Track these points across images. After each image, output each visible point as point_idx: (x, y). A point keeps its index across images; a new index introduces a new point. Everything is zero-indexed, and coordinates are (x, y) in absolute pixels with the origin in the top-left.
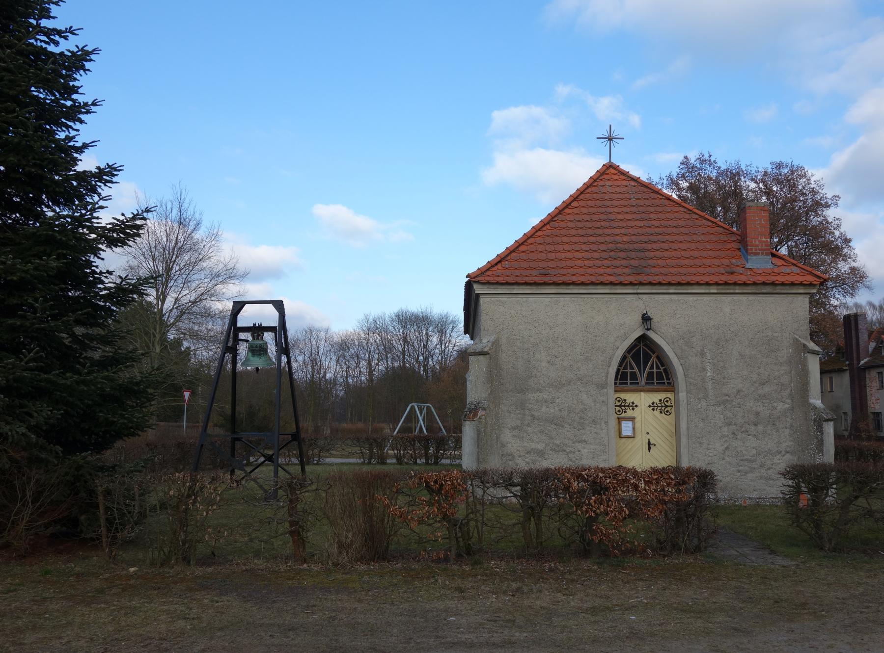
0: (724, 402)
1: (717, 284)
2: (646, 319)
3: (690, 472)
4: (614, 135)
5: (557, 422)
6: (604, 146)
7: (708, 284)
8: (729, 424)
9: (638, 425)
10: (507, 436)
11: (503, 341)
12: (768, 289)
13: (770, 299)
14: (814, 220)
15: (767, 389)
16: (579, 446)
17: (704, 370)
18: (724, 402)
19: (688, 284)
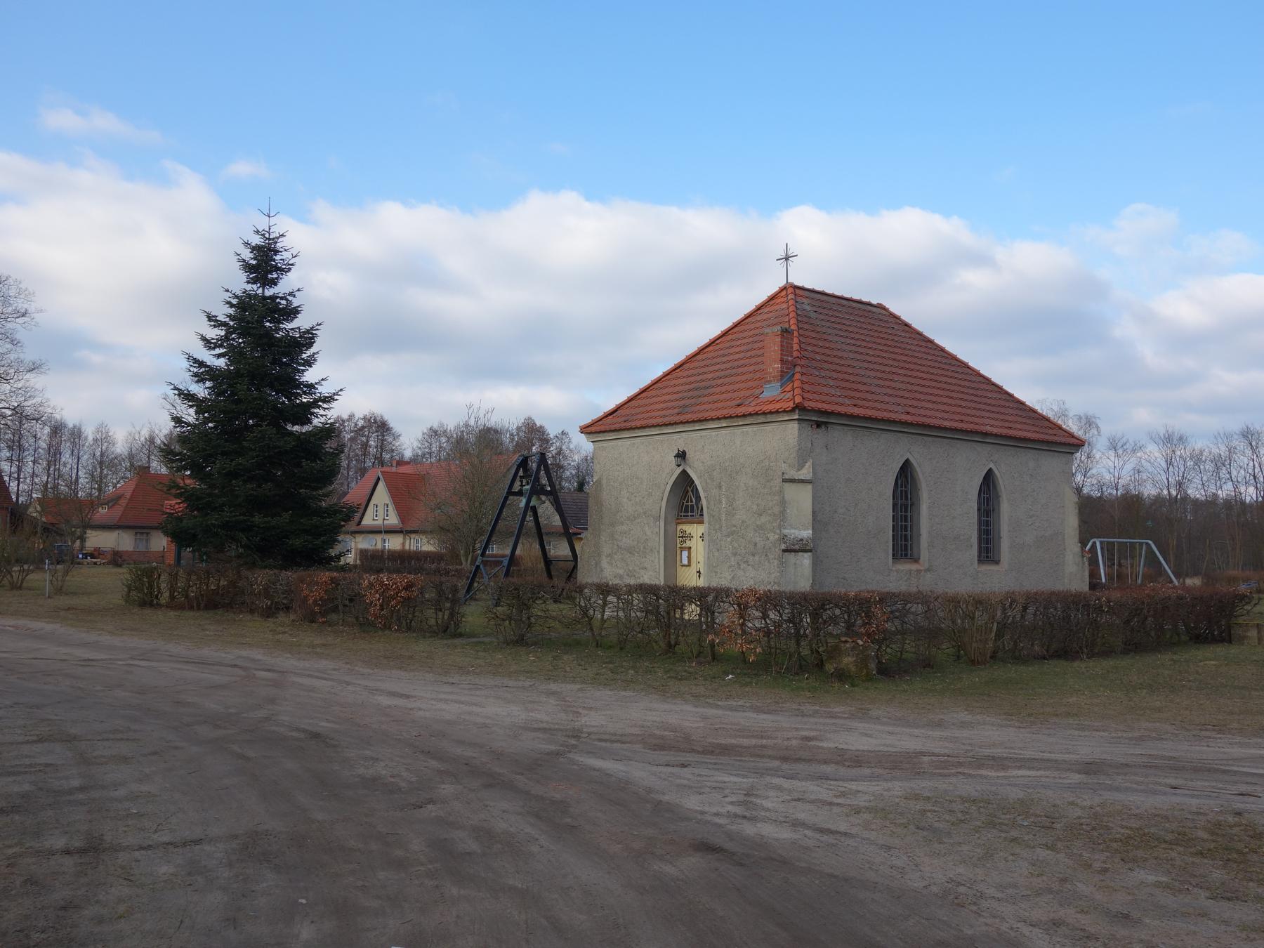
0: (733, 533)
1: (725, 418)
2: (682, 455)
3: (843, 602)
4: (790, 254)
5: (631, 550)
6: (781, 266)
7: (718, 419)
8: (735, 554)
9: (693, 554)
10: (604, 563)
11: (604, 482)
12: (761, 419)
13: (768, 428)
14: (187, 479)
15: (763, 519)
16: (642, 572)
17: (721, 502)
18: (733, 533)
19: (706, 420)
